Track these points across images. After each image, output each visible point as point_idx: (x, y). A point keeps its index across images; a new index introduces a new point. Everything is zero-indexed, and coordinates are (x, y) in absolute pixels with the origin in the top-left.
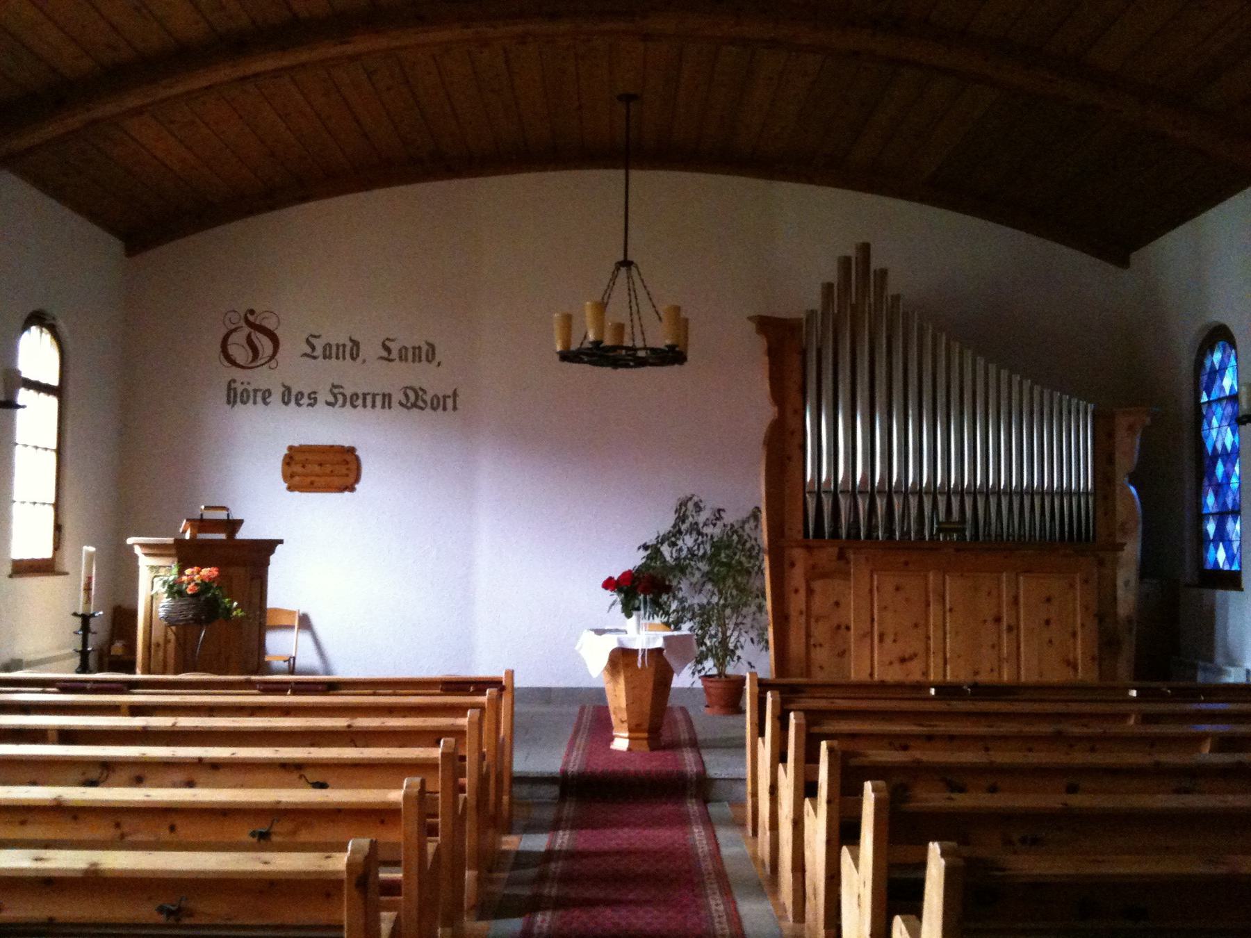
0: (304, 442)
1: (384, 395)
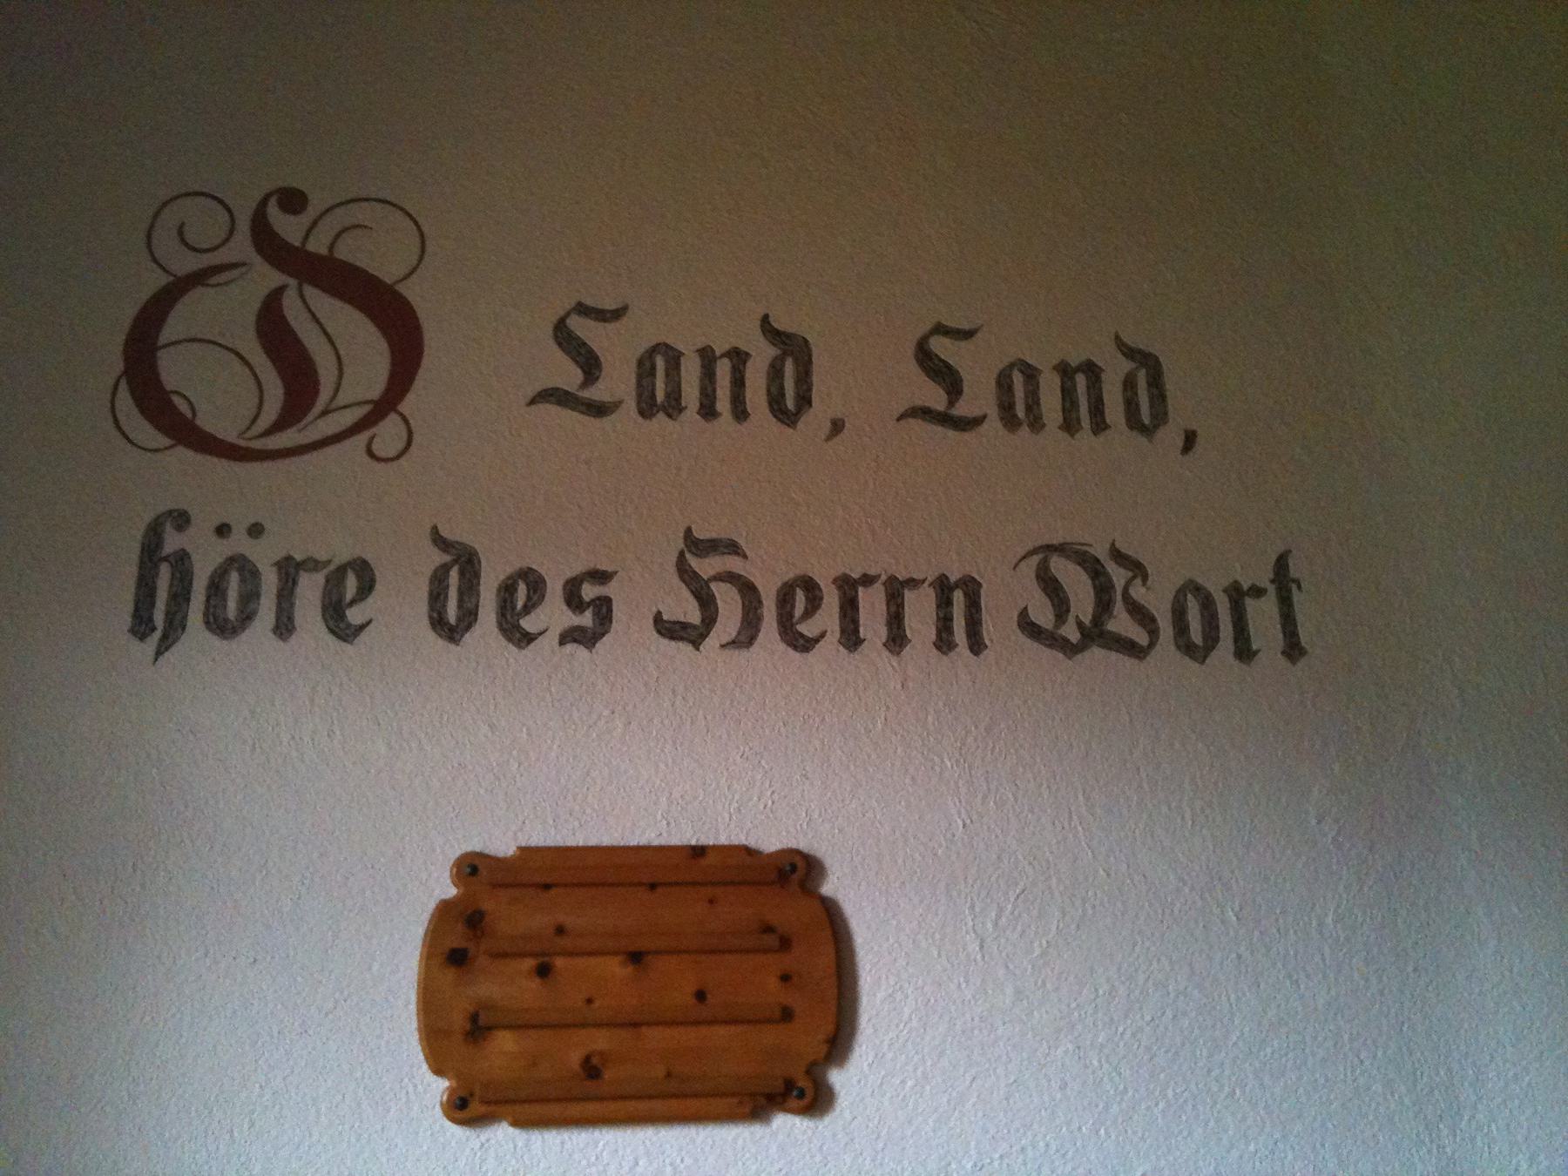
0: (539, 836)
1: (944, 588)
